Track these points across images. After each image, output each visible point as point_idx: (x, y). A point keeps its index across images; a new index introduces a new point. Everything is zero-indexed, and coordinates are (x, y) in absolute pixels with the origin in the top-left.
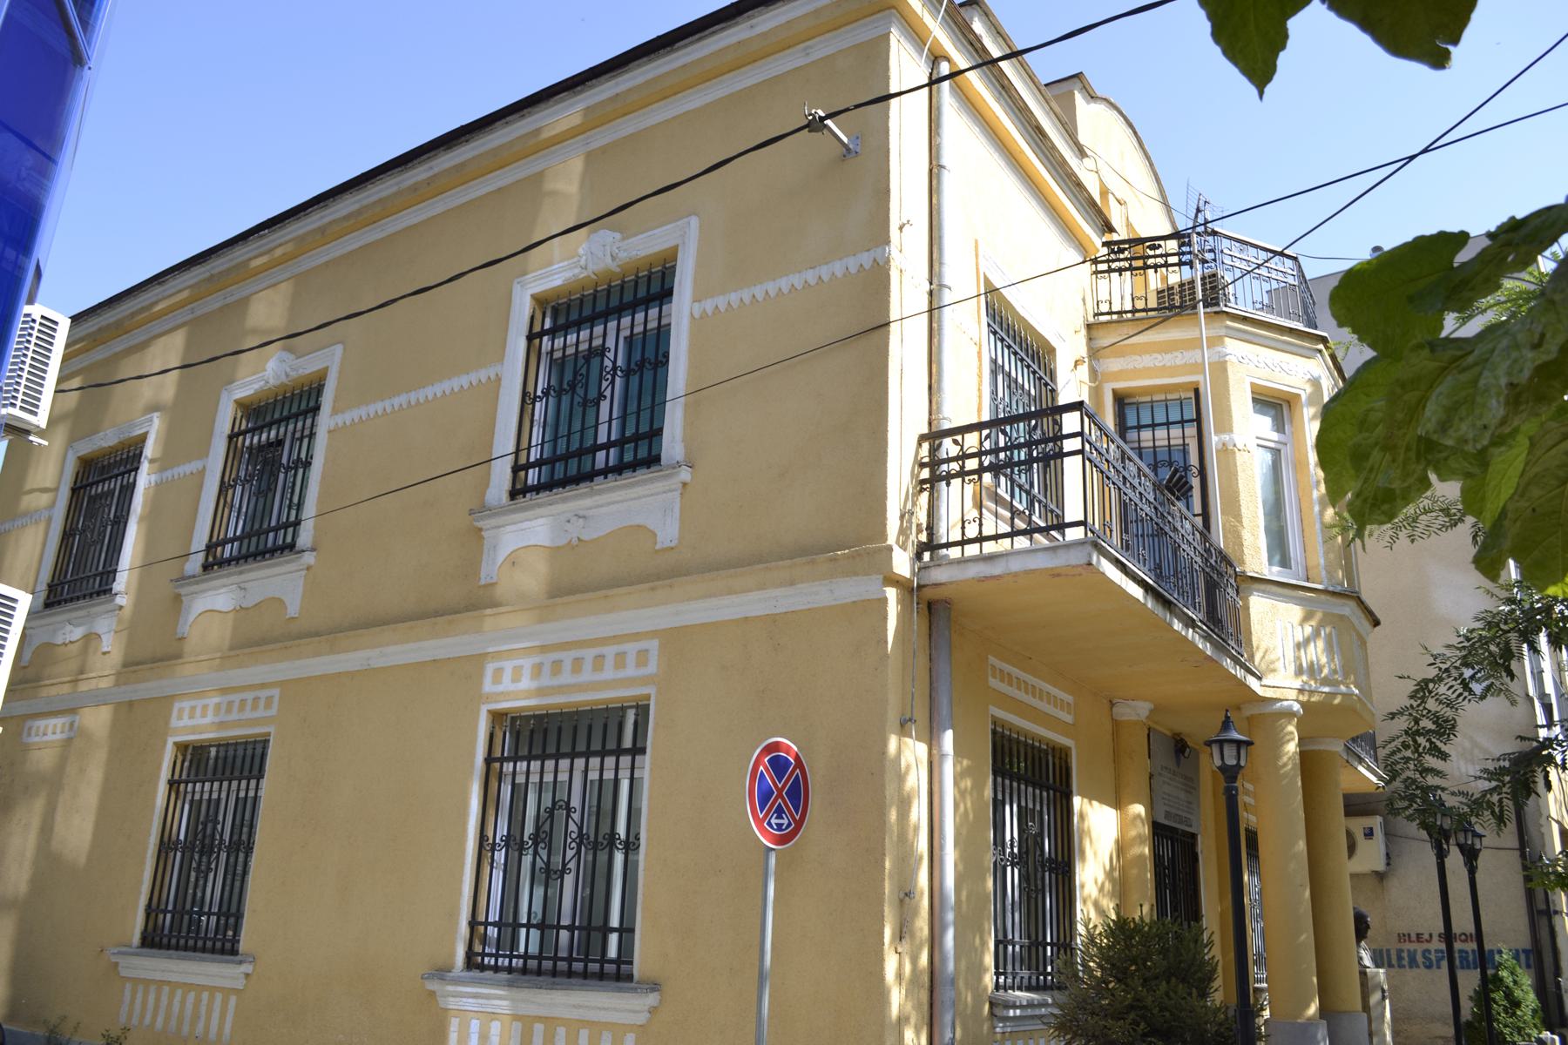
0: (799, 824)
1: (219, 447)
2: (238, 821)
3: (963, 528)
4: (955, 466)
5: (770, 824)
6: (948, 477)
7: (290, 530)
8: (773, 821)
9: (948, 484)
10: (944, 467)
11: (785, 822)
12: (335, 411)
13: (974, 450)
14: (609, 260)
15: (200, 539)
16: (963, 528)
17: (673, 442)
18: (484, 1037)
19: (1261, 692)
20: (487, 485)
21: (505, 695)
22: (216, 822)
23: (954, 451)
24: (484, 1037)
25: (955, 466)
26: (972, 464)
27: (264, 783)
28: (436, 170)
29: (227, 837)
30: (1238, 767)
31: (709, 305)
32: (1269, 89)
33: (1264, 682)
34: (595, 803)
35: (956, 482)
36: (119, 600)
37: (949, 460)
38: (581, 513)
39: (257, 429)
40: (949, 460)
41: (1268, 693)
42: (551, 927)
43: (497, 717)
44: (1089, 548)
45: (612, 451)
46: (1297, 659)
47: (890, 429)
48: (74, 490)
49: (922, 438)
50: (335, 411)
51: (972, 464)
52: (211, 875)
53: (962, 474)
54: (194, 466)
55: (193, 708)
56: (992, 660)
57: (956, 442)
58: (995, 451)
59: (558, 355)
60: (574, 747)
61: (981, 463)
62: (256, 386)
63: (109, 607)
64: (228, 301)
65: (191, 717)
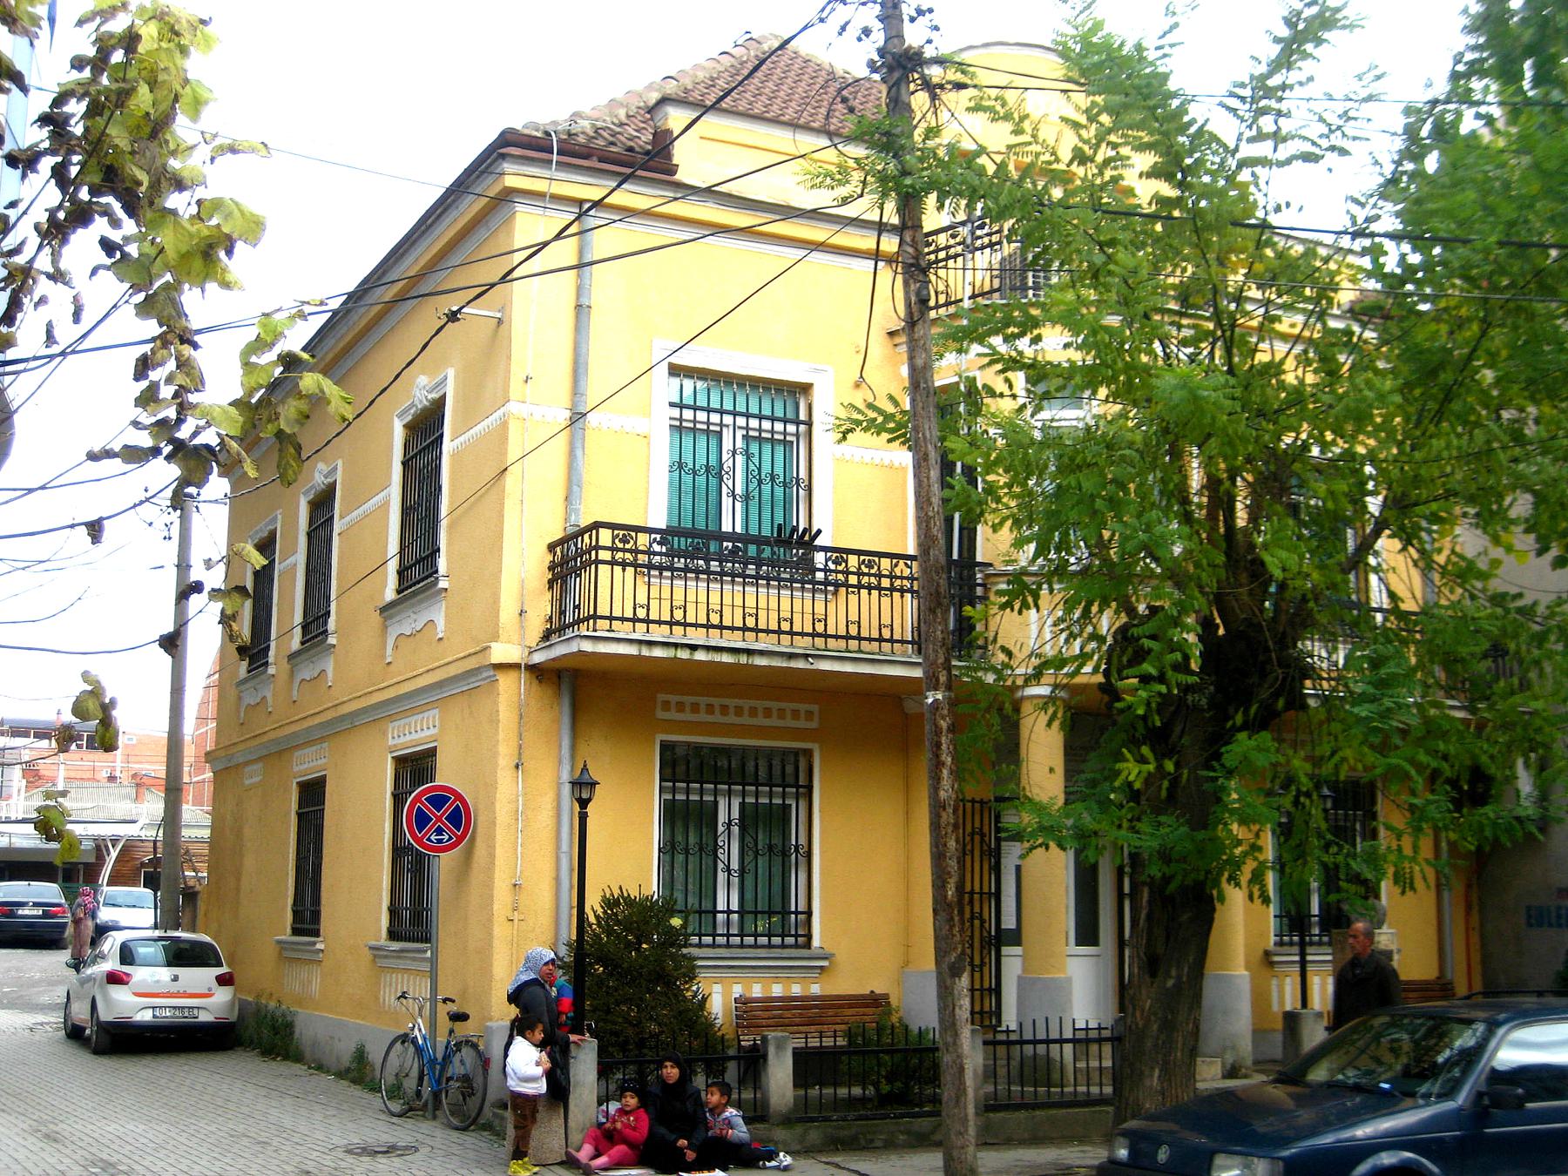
12: (342, 517)
36: (332, 640)
43: (400, 761)
50: (342, 517)
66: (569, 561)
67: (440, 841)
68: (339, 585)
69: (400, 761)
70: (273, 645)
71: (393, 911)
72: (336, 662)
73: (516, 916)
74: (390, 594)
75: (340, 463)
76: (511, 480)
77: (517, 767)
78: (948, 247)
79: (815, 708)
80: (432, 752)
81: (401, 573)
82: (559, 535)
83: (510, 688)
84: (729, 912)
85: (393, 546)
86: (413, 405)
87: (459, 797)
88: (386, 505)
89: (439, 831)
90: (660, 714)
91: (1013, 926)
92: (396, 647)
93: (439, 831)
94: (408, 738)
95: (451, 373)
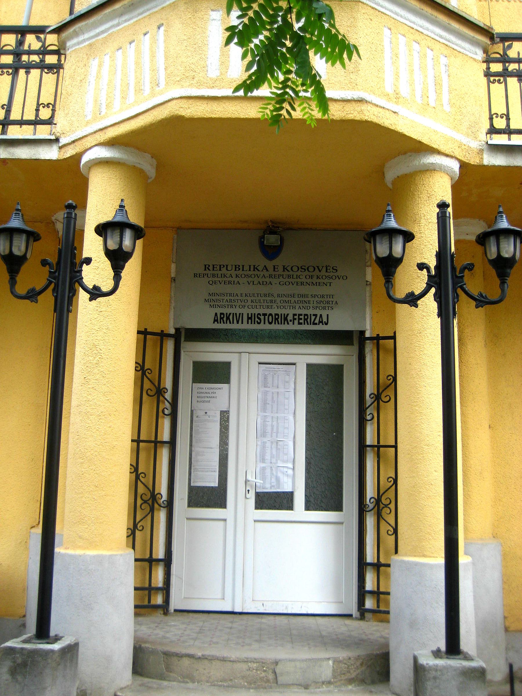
3: (37, 110)
4: (35, 58)
6: (28, 67)
9: (28, 73)
16: (37, 110)
18: (519, 61)
23: (36, 45)
24: (519, 61)
25: (35, 58)
30: (23, 259)
32: (60, 635)
33: (63, 141)
35: (35, 73)
37: (30, 53)
38: (335, 271)
40: (30, 53)
41: (69, 152)
46: (356, 619)
47: (459, 544)
57: (38, 38)
91: (215, 483)
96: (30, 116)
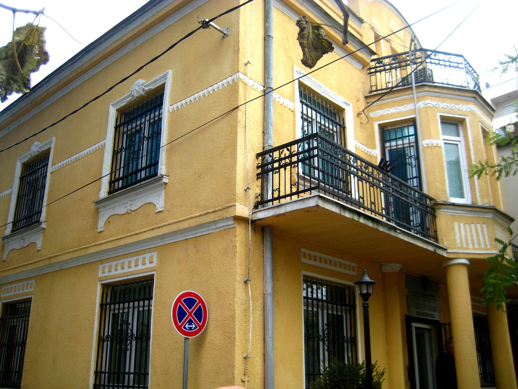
0: (201, 327)
1: (17, 182)
2: (140, 324)
4: (287, 161)
5: (185, 327)
7: (153, 168)
8: (187, 326)
10: (283, 162)
11: (194, 326)
12: (53, 164)
13: (277, 159)
14: (142, 92)
15: (11, 218)
17: (162, 169)
19: (445, 255)
20: (100, 190)
21: (107, 278)
22: (128, 324)
26: (295, 159)
27: (153, 302)
28: (83, 62)
29: (135, 332)
31: (175, 106)
34: (141, 321)
36: (44, 226)
39: (127, 123)
42: (137, 374)
43: (105, 286)
44: (317, 198)
45: (147, 170)
48: (116, 128)
49: (258, 155)
50: (53, 164)
51: (295, 159)
52: (128, 352)
53: (291, 164)
54: (7, 192)
55: (110, 267)
56: (303, 250)
57: (270, 156)
58: (304, 152)
59: (152, 121)
60: (144, 296)
61: (298, 158)
62: (28, 157)
63: (38, 229)
64: (20, 123)
65: (144, 264)
66: (266, 165)
67: (190, 329)
68: (49, 199)
69: (105, 286)
70: (44, 210)
71: (97, 373)
72: (166, 194)
73: (246, 379)
74: (104, 193)
75: (54, 139)
76: (240, 114)
77: (246, 282)
78: (375, 68)
79: (355, 265)
80: (151, 279)
81: (111, 183)
82: (260, 151)
83: (241, 235)
84: (129, 373)
85: (107, 169)
86: (130, 95)
87: (201, 301)
88: (102, 150)
89: (190, 322)
90: (303, 260)
92: (108, 222)
93: (190, 322)
94: (21, 291)
95: (170, 73)
96: (288, 192)
